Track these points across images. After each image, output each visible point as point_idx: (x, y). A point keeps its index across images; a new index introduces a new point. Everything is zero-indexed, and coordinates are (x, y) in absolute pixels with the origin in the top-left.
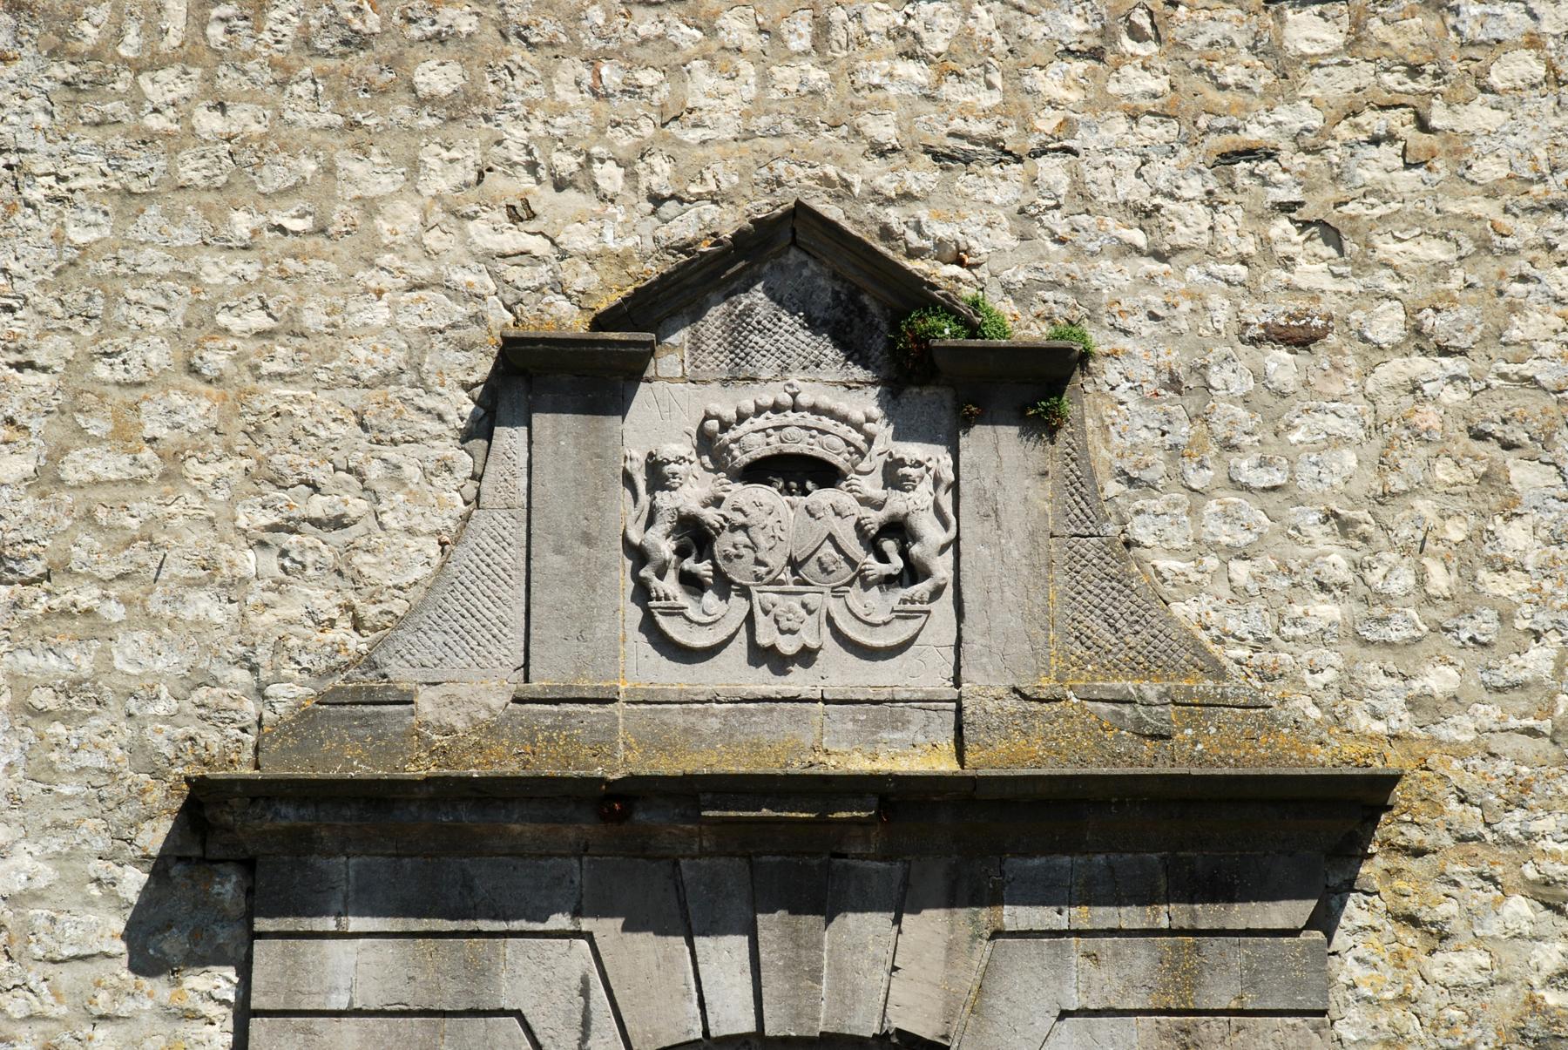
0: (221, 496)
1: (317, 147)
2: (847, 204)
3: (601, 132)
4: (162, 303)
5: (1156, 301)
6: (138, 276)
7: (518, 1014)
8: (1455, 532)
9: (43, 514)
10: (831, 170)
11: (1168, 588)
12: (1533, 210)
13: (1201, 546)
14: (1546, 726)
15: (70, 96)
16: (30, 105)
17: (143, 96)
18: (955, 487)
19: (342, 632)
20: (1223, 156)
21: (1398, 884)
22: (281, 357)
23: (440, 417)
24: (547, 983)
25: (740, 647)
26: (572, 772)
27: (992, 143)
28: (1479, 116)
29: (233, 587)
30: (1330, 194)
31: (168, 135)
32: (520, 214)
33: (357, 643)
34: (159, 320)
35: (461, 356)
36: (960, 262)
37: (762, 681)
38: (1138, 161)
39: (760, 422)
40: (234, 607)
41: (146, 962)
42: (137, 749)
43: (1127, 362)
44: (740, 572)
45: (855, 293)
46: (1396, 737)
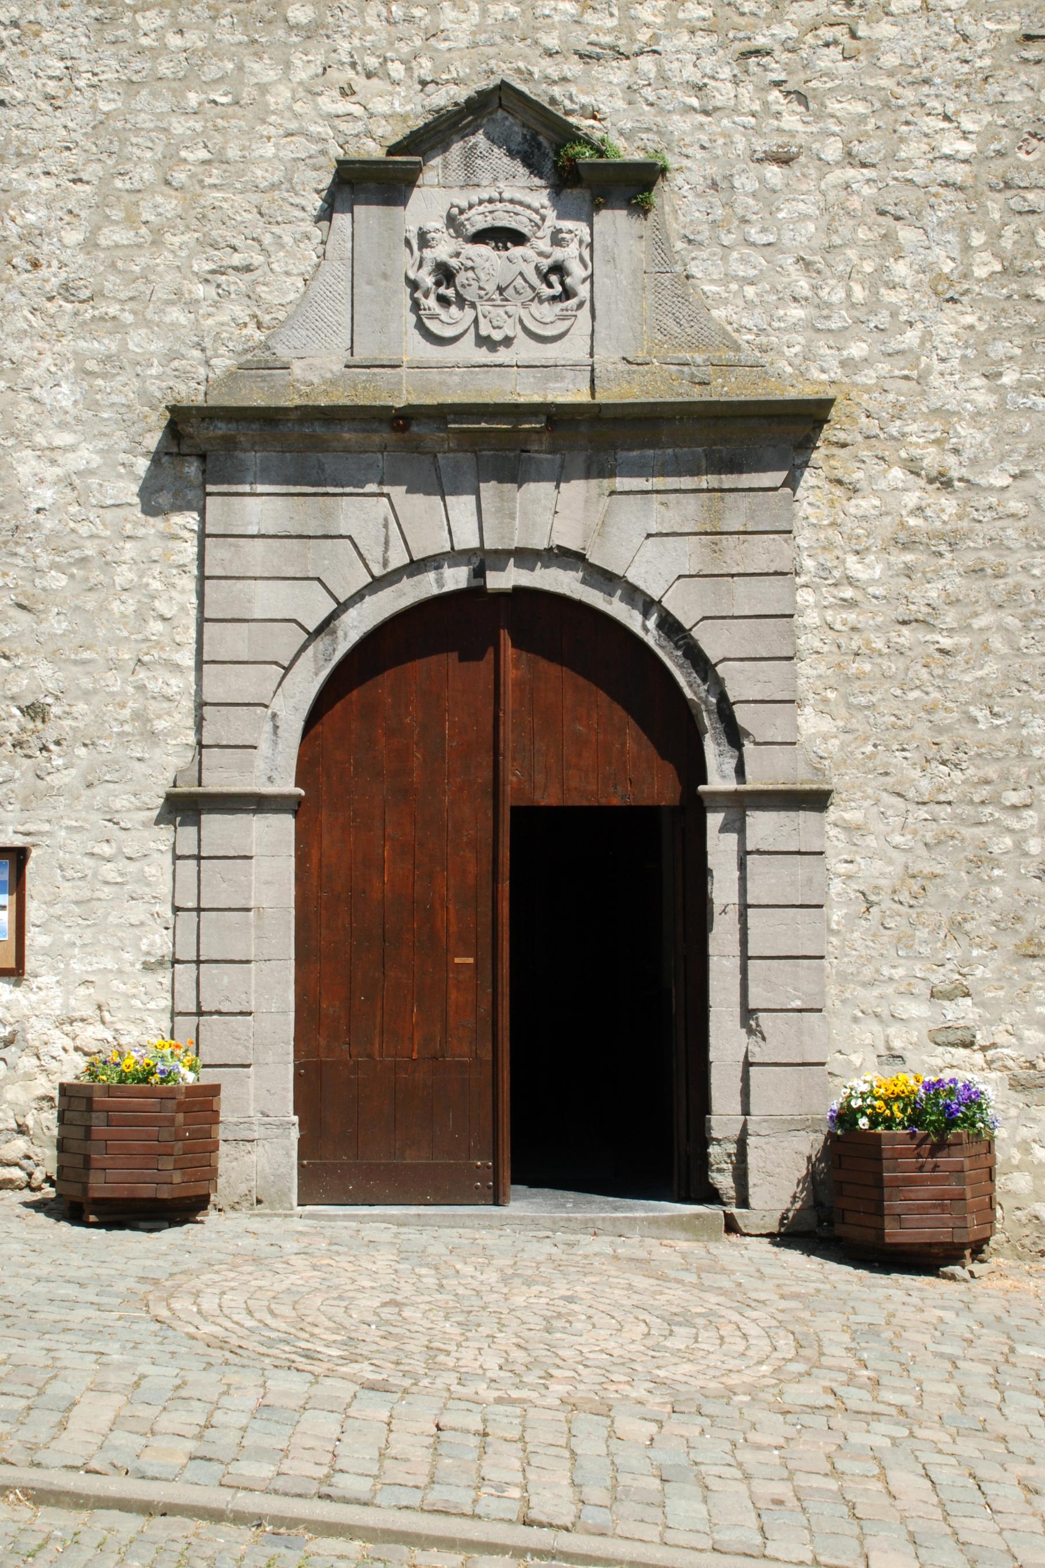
0: (184, 254)
1: (234, 55)
2: (531, 85)
3: (392, 44)
4: (150, 145)
5: (704, 138)
6: (137, 130)
7: (350, 538)
8: (868, 267)
9: (89, 263)
10: (521, 65)
11: (710, 301)
12: (913, 83)
13: (729, 277)
14: (914, 374)
15: (99, 27)
16: (78, 32)
17: (138, 26)
18: (591, 245)
19: (251, 330)
20: (743, 54)
21: (833, 463)
22: (215, 177)
23: (303, 209)
24: (365, 521)
25: (471, 336)
26: (377, 403)
27: (613, 48)
28: (885, 29)
29: (191, 305)
30: (802, 76)
31: (152, 48)
32: (347, 92)
33: (259, 336)
34: (148, 154)
35: (314, 174)
36: (595, 118)
37: (483, 355)
38: (694, 57)
39: (481, 209)
40: (192, 316)
41: (150, 509)
42: (142, 393)
43: (688, 174)
44: (469, 295)
45: (535, 135)
46: (833, 382)
